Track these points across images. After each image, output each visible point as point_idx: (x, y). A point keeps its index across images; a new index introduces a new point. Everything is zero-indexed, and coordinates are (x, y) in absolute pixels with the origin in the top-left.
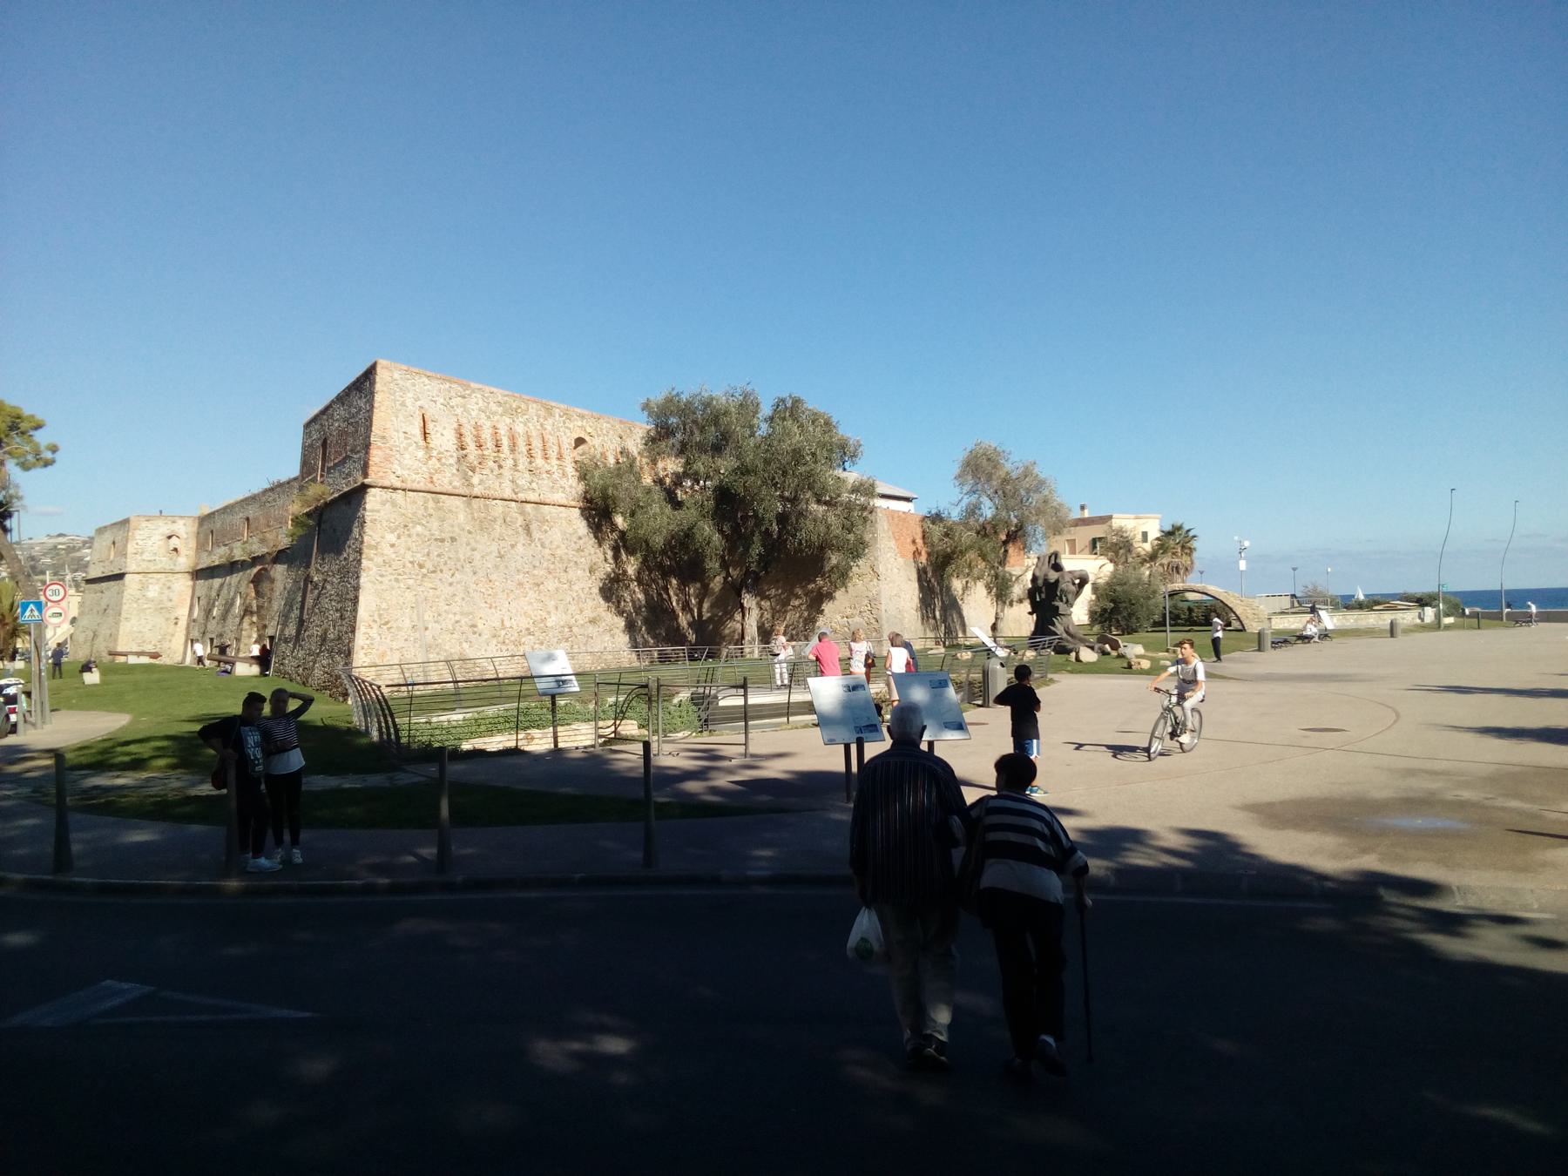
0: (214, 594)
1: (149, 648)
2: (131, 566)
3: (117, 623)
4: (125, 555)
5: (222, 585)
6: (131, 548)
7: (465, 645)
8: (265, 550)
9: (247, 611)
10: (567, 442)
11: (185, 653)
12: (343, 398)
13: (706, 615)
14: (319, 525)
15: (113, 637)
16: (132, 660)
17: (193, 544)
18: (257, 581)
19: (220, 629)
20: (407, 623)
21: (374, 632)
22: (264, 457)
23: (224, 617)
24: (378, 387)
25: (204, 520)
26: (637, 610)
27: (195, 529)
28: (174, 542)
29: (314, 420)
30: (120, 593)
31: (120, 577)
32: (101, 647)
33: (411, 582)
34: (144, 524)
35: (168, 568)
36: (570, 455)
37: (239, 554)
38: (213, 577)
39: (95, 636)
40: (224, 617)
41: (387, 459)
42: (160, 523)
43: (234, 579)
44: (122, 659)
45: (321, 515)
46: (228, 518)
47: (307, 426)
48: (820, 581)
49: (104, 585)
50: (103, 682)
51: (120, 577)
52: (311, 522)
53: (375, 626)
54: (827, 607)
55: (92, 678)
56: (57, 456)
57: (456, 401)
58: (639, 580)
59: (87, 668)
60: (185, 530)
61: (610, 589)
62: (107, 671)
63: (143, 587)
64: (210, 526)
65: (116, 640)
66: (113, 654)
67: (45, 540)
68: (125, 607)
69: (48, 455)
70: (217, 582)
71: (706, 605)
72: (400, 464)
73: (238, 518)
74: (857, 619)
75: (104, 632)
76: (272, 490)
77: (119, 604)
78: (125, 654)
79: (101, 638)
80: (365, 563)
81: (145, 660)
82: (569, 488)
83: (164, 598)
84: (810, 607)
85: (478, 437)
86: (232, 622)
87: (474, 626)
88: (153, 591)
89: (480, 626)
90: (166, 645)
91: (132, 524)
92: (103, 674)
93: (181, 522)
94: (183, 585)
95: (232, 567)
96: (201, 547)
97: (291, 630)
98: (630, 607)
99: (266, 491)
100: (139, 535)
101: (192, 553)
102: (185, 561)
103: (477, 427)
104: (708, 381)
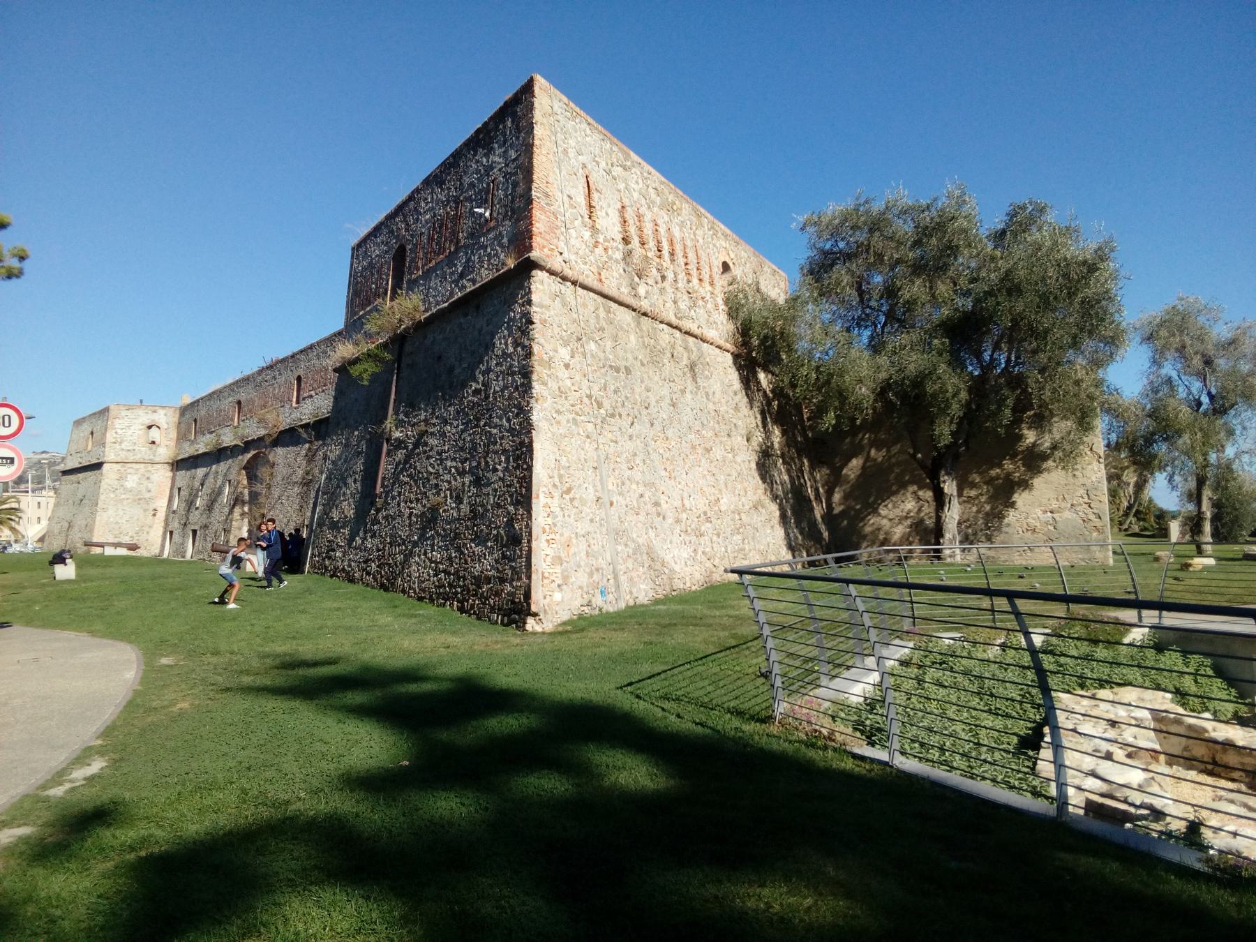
0: (197, 484)
1: (126, 539)
2: (110, 454)
3: (93, 513)
4: (104, 445)
5: (206, 475)
6: (110, 437)
7: (652, 534)
8: (262, 432)
9: (237, 501)
10: (717, 268)
11: (163, 546)
12: (481, 140)
13: (837, 509)
14: (399, 360)
15: (89, 528)
16: (109, 551)
17: (173, 434)
18: (251, 470)
19: (204, 520)
20: (591, 495)
21: (555, 504)
22: (288, 307)
23: (210, 508)
24: (538, 115)
25: (184, 411)
26: (786, 494)
27: (176, 420)
28: (154, 434)
29: (359, 245)
30: (98, 483)
31: (98, 466)
32: (76, 540)
33: (590, 427)
34: (124, 413)
35: (147, 458)
36: (721, 282)
37: (228, 439)
38: (196, 467)
39: (70, 526)
40: (210, 508)
41: (553, 229)
42: (141, 412)
43: (222, 467)
44: (98, 550)
45: (402, 346)
46: (215, 405)
47: (356, 249)
48: (1008, 465)
49: (81, 476)
50: (81, 578)
51: (98, 466)
52: (388, 356)
53: (556, 494)
54: (1021, 498)
55: (66, 572)
56: (26, 265)
57: (617, 171)
58: (783, 456)
59: (59, 558)
60: (167, 419)
61: (764, 465)
62: (82, 563)
63: (121, 478)
64: (193, 417)
65: (91, 531)
66: (88, 544)
67: (31, 455)
68: (102, 497)
69: (14, 263)
70: (201, 472)
71: (837, 497)
72: (567, 243)
73: (228, 403)
74: (1068, 514)
75: (80, 522)
76: (270, 367)
77: (96, 494)
78: (101, 545)
79: (76, 529)
80: (537, 388)
81: (123, 552)
82: (720, 328)
83: (143, 488)
84: (993, 498)
85: (641, 237)
86: (219, 514)
87: (657, 504)
88: (132, 482)
89: (664, 506)
90: (143, 537)
91: (112, 413)
92: (78, 567)
93: (162, 412)
94: (163, 476)
95: (219, 454)
96: (182, 437)
97: (347, 508)
98: (780, 493)
99: (261, 371)
100: (118, 424)
101: (173, 444)
102: (166, 451)
103: (640, 217)
104: (901, 188)
